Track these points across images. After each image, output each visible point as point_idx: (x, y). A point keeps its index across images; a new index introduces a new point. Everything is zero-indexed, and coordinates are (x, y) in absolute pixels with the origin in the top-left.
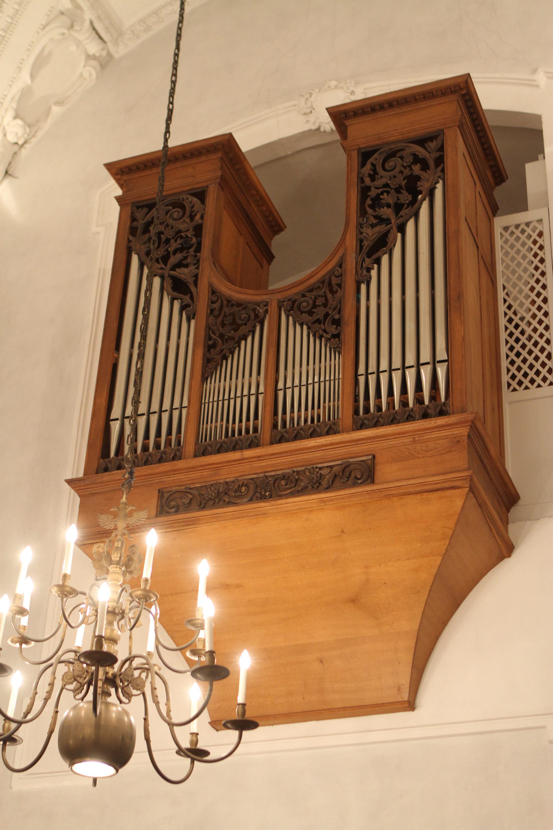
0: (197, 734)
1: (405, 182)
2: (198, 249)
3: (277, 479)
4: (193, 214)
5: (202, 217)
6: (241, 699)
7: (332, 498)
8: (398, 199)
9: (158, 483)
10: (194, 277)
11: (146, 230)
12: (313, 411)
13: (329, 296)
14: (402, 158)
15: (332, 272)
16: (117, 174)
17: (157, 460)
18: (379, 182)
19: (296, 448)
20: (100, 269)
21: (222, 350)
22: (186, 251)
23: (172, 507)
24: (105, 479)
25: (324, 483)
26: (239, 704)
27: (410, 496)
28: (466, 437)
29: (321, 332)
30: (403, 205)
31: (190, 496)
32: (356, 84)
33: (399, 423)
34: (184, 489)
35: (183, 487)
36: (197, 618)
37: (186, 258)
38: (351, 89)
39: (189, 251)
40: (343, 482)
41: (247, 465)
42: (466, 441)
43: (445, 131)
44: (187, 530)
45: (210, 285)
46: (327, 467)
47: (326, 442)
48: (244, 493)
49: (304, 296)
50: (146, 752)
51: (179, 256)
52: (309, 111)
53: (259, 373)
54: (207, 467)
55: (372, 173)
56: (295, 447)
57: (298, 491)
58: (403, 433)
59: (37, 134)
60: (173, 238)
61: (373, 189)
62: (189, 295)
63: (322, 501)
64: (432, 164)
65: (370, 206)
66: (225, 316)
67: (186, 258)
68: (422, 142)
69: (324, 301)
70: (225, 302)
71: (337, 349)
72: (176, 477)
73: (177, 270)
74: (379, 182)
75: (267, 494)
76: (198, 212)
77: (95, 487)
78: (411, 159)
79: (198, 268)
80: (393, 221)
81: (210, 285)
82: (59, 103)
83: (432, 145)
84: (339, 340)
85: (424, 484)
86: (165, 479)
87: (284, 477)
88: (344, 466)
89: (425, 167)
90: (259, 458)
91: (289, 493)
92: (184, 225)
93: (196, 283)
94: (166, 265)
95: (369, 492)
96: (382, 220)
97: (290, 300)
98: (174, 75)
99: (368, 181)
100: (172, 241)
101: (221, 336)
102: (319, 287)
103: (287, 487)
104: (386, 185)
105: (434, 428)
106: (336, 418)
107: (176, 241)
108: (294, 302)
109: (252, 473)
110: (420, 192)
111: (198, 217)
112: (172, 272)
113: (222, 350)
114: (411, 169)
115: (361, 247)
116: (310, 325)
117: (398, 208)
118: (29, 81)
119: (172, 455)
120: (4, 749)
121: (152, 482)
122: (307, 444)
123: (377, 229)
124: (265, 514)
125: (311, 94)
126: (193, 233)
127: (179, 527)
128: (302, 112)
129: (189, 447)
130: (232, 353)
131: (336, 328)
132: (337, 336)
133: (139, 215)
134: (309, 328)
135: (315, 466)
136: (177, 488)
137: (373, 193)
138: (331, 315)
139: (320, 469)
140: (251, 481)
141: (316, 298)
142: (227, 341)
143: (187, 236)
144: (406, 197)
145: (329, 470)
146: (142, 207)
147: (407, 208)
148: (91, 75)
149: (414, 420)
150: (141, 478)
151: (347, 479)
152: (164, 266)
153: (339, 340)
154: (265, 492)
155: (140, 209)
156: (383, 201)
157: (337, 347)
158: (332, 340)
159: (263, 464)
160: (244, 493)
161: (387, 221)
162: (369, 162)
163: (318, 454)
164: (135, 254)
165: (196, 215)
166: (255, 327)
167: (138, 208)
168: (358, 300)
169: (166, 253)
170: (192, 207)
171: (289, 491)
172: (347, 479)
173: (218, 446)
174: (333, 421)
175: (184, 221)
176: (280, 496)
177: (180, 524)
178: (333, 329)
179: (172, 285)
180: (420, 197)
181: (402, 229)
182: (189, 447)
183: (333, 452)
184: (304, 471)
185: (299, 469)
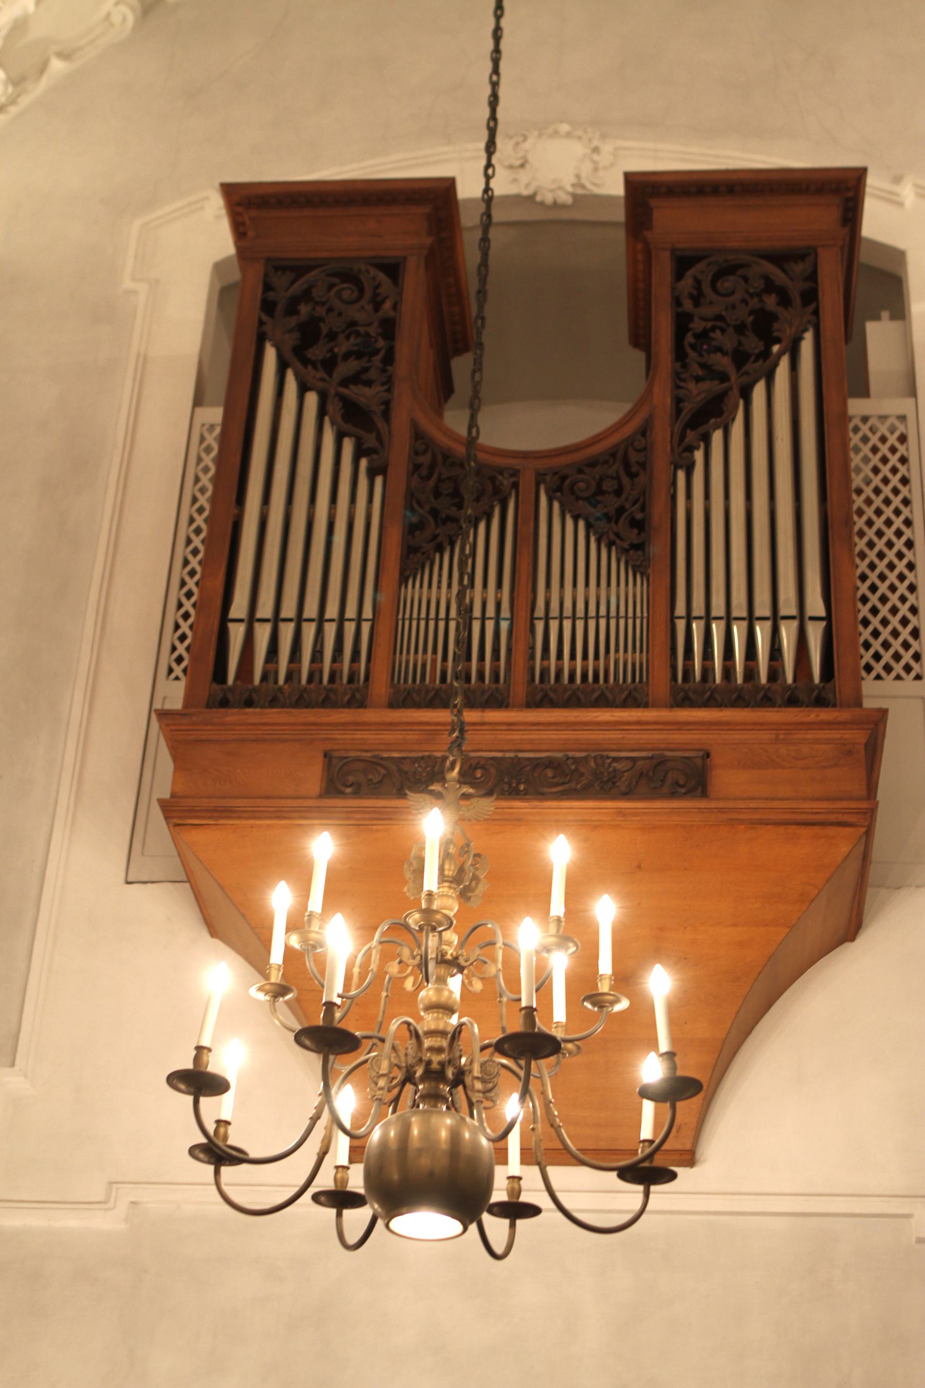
0: (520, 1178)
1: (751, 319)
2: (389, 358)
3: (537, 764)
4: (379, 299)
5: (395, 307)
6: (646, 1132)
7: (638, 810)
8: (740, 344)
9: (324, 739)
10: (382, 404)
11: (291, 310)
12: (596, 662)
13: (625, 480)
14: (746, 279)
15: (629, 442)
16: (239, 204)
17: (320, 701)
18: (707, 311)
19: (579, 719)
20: (138, 355)
21: (435, 537)
22: (366, 359)
23: (349, 784)
24: (229, 719)
25: (622, 785)
26: (644, 1141)
27: (769, 827)
28: (862, 747)
29: (612, 537)
30: (749, 356)
31: (383, 771)
32: (604, 137)
33: (747, 706)
34: (370, 757)
35: (369, 754)
36: (600, 991)
37: (365, 370)
38: (596, 143)
39: (373, 359)
40: (655, 788)
41: (487, 734)
42: (863, 752)
43: (819, 250)
44: (374, 827)
45: (415, 425)
46: (627, 758)
47: (630, 719)
48: (480, 780)
49: (580, 471)
50: (209, 1184)
51: (353, 365)
52: (518, 163)
53: (499, 585)
54: (415, 728)
55: (695, 293)
56: (576, 717)
57: (576, 790)
58: (761, 724)
59: (19, 100)
60: (343, 331)
61: (696, 319)
62: (374, 434)
63: (621, 813)
64: (797, 300)
65: (693, 347)
66: (439, 480)
67: (365, 370)
68: (780, 258)
69: (616, 487)
70: (439, 458)
71: (640, 568)
72: (358, 735)
73: (352, 387)
74: (707, 311)
75: (522, 787)
76: (387, 297)
77: (209, 730)
78: (760, 284)
79: (389, 390)
80: (733, 378)
81: (415, 425)
82: (65, 56)
83: (799, 268)
84: (644, 555)
85: (797, 810)
86: (338, 735)
87: (550, 763)
88: (655, 762)
89: (785, 300)
90: (511, 726)
91: (560, 792)
92: (361, 313)
93: (386, 415)
94: (330, 373)
95: (702, 810)
96: (712, 373)
97: (555, 473)
98: (496, 71)
99: (688, 305)
100: (341, 337)
101: (434, 512)
102: (606, 462)
103: (555, 780)
104: (719, 318)
105: (812, 723)
106: (637, 679)
107: (348, 337)
108: (564, 478)
109: (494, 749)
110: (778, 341)
111: (388, 305)
112: (342, 390)
113: (435, 537)
114: (761, 301)
115: (678, 411)
116: (592, 520)
117: (740, 358)
118: (31, 8)
119: (347, 697)
120: (217, 1173)
121: (314, 737)
122: (597, 717)
123: (706, 385)
124: (519, 820)
125: (525, 138)
126: (380, 331)
127: (364, 819)
128: (507, 163)
129: (380, 688)
130: (452, 545)
131: (639, 534)
132: (639, 547)
133: (281, 281)
134: (589, 527)
135: (605, 753)
136: (358, 754)
137: (697, 325)
138: (629, 512)
139: (615, 759)
140: (491, 762)
141: (601, 480)
142: (444, 523)
143: (367, 334)
144: (753, 344)
145: (629, 764)
146: (284, 269)
147: (755, 361)
148: (124, 20)
149: (773, 706)
150: (294, 727)
151: (660, 783)
152: (326, 377)
153: (644, 555)
154: (518, 783)
155: (279, 273)
156: (714, 343)
157: (640, 566)
158: (632, 552)
159: (516, 736)
160: (480, 780)
161: (723, 377)
162: (690, 273)
163: (613, 735)
164: (272, 345)
165: (383, 301)
166: (492, 507)
167: (277, 269)
168: (674, 498)
169: (329, 355)
170: (377, 287)
171: (559, 788)
172: (660, 783)
173: (431, 694)
174: (633, 686)
175: (362, 308)
176: (543, 794)
177: (367, 816)
178: (633, 536)
179: (342, 411)
180: (776, 348)
181: (746, 393)
182: (380, 688)
183: (638, 736)
184: (586, 758)
185: (578, 755)
